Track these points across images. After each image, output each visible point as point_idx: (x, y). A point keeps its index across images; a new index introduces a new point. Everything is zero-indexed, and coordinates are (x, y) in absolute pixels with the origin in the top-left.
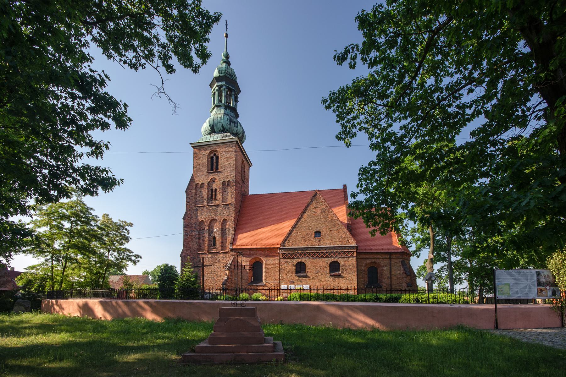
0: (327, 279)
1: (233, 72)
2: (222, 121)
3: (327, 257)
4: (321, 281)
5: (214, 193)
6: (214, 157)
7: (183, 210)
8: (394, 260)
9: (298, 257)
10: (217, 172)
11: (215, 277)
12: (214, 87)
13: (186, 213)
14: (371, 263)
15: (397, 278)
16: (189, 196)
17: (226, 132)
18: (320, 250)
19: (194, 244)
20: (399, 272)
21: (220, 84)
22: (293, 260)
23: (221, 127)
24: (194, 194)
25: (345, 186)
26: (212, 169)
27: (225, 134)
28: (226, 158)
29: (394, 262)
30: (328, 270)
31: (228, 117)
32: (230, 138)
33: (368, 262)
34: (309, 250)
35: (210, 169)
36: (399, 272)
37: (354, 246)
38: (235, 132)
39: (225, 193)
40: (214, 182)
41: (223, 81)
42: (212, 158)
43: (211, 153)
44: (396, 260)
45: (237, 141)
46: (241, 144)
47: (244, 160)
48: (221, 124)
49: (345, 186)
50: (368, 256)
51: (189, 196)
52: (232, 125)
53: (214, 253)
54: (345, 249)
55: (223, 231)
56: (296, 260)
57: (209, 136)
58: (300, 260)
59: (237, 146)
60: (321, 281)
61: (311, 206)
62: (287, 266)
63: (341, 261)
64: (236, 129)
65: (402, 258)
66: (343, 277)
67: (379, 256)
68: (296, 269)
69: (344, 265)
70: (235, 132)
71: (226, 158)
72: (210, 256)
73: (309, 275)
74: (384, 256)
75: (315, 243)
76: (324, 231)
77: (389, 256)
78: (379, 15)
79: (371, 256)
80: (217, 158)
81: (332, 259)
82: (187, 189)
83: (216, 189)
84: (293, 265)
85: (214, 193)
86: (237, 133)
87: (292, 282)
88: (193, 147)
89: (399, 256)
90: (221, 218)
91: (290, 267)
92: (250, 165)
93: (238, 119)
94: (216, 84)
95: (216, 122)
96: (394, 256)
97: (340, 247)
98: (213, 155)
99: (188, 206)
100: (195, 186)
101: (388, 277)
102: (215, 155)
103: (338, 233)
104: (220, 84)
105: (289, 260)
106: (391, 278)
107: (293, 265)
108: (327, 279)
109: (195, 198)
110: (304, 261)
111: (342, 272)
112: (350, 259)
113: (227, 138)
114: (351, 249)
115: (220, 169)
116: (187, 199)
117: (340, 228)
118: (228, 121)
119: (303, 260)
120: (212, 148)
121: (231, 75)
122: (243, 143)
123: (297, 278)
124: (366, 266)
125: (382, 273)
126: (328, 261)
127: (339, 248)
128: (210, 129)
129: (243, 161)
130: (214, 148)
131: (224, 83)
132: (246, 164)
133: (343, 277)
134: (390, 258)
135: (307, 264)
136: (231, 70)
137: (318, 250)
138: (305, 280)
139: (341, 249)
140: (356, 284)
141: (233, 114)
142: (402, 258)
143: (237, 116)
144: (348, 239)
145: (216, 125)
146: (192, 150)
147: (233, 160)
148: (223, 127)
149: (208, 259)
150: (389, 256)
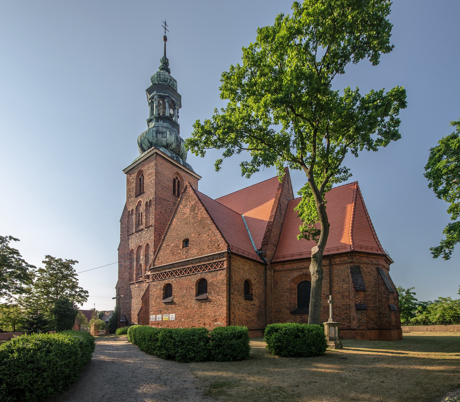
4: (187, 308)
5: (140, 218)
7: (118, 242)
8: (338, 267)
13: (120, 243)
14: (300, 276)
16: (123, 226)
18: (186, 265)
19: (127, 275)
20: (345, 286)
23: (148, 143)
24: (127, 223)
28: (149, 175)
29: (337, 270)
30: (194, 292)
33: (296, 274)
34: (175, 267)
36: (345, 286)
37: (224, 253)
38: (164, 143)
39: (148, 215)
40: (140, 205)
43: (139, 175)
44: (342, 267)
48: (146, 139)
50: (295, 266)
53: (139, 282)
54: (213, 259)
55: (147, 256)
56: (164, 281)
58: (167, 282)
60: (187, 308)
61: (180, 206)
63: (209, 278)
64: (165, 139)
65: (352, 262)
66: (210, 301)
69: (212, 283)
71: (149, 175)
73: (175, 300)
76: (192, 237)
77: (328, 262)
86: (168, 144)
87: (161, 312)
88: (126, 173)
89: (346, 258)
90: (145, 243)
91: (158, 292)
96: (337, 260)
97: (207, 257)
98: (140, 176)
100: (127, 214)
103: (208, 237)
109: (128, 227)
111: (210, 293)
112: (219, 272)
114: (220, 258)
116: (121, 229)
117: (210, 229)
118: (154, 132)
121: (165, 81)
124: (293, 281)
126: (194, 279)
127: (207, 259)
133: (210, 301)
134: (331, 265)
135: (173, 286)
137: (184, 266)
139: (209, 260)
142: (352, 262)
144: (219, 243)
147: (154, 176)
150: (328, 262)
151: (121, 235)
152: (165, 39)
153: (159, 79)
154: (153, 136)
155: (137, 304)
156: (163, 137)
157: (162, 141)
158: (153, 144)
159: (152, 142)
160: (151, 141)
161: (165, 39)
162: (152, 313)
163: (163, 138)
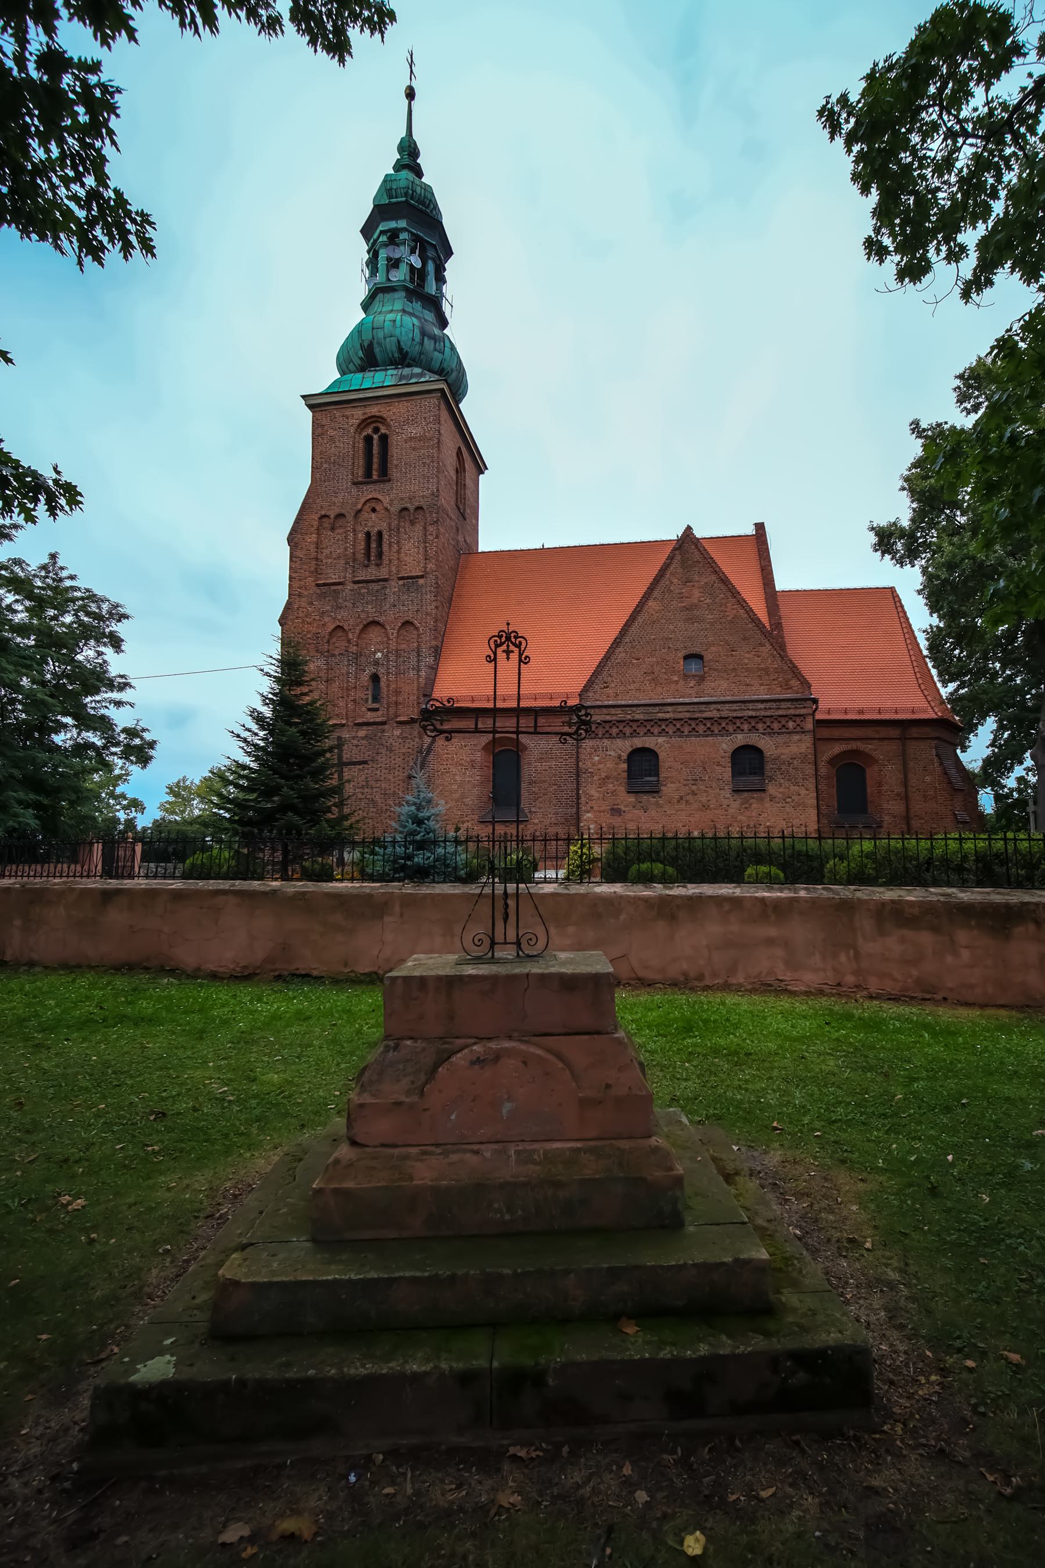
0: (726, 802)
1: (429, 197)
2: (398, 332)
3: (724, 732)
5: (374, 545)
6: (375, 437)
9: (634, 734)
10: (384, 482)
11: (378, 798)
12: (375, 236)
15: (925, 796)
17: (409, 366)
20: (928, 779)
21: (393, 224)
22: (619, 742)
23: (395, 349)
24: (312, 547)
25: (760, 527)
26: (368, 473)
27: (407, 371)
30: (727, 773)
31: (415, 321)
32: (423, 380)
33: (838, 748)
35: (361, 472)
36: (928, 779)
38: (436, 365)
41: (401, 218)
42: (368, 440)
45: (442, 390)
46: (457, 402)
47: (464, 450)
49: (760, 527)
50: (837, 732)
51: (300, 554)
52: (428, 344)
57: (359, 375)
58: (638, 742)
59: (443, 406)
62: (600, 762)
63: (767, 744)
64: (440, 356)
67: (869, 732)
68: (629, 771)
70: (436, 365)
72: (362, 733)
74: (884, 732)
75: (688, 691)
78: (13, 1202)
79: (847, 732)
80: (384, 439)
81: (740, 739)
82: (291, 534)
83: (380, 534)
84: (619, 757)
85: (374, 545)
86: (443, 370)
92: (480, 467)
93: (446, 331)
94: (381, 228)
95: (380, 334)
96: (914, 732)
98: (369, 431)
99: (296, 585)
101: (898, 795)
102: (376, 430)
104: (393, 224)
105: (606, 742)
106: (906, 798)
107: (619, 757)
108: (726, 802)
110: (651, 746)
112: (796, 737)
113: (413, 381)
115: (394, 473)
116: (291, 560)
118: (417, 331)
119: (649, 742)
120: (367, 410)
121: (423, 203)
122: (460, 401)
123: (632, 799)
125: (880, 784)
126: (727, 744)
128: (361, 354)
129: (459, 453)
130: (374, 410)
131: (402, 224)
132: (469, 464)
135: (662, 755)
136: (428, 189)
138: (657, 804)
140: (813, 813)
141: (430, 316)
143: (443, 323)
145: (379, 344)
146: (309, 414)
148: (400, 349)
149: (355, 742)
151: (291, 578)
152: (410, 94)
153: (410, 192)
154: (413, 340)
155: (363, 787)
156: (435, 350)
157: (432, 359)
158: (409, 357)
159: (407, 352)
160: (405, 348)
161: (410, 94)
162: (589, 815)
163: (436, 353)
